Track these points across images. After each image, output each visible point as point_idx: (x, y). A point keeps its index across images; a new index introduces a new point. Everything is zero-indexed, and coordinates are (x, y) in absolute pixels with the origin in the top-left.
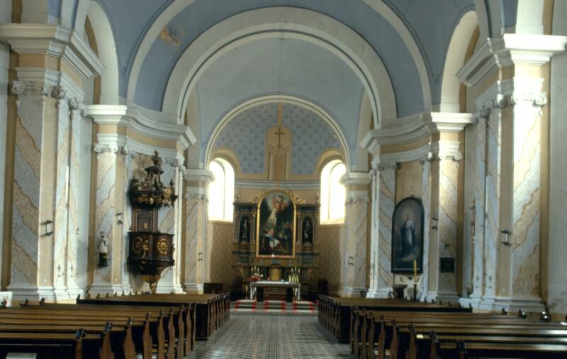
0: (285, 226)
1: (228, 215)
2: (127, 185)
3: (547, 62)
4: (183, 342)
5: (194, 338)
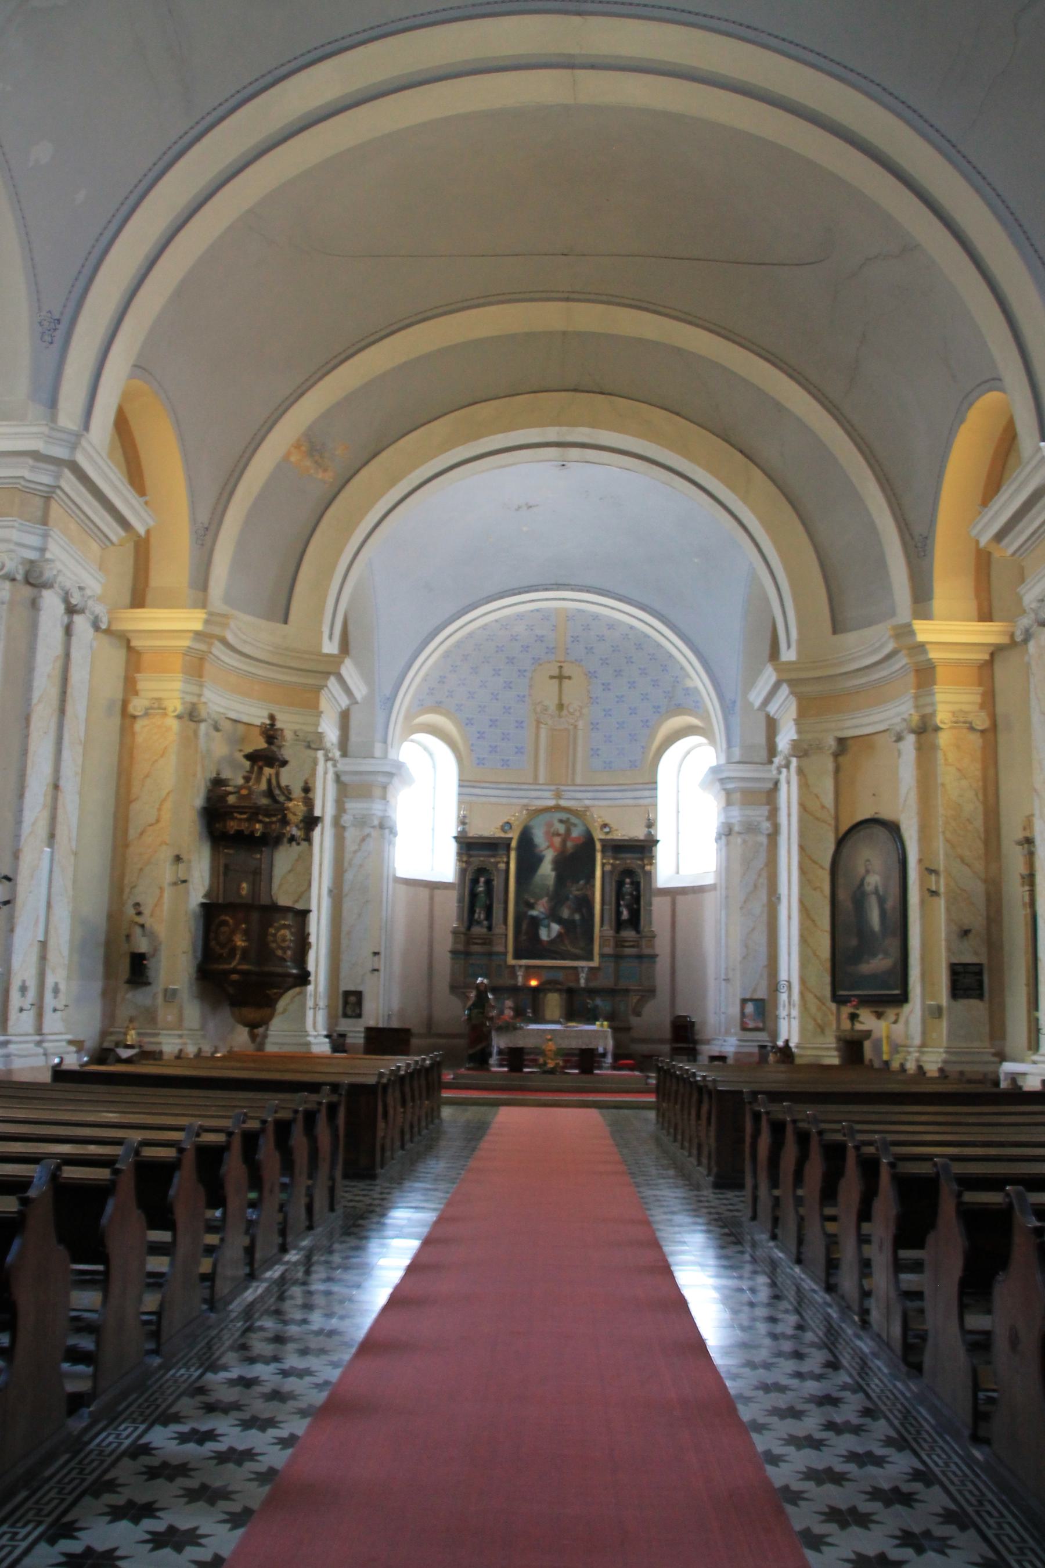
0: (575, 891)
1: (441, 864)
3: (986, 661)
4: (303, 1191)
5: (338, 1173)
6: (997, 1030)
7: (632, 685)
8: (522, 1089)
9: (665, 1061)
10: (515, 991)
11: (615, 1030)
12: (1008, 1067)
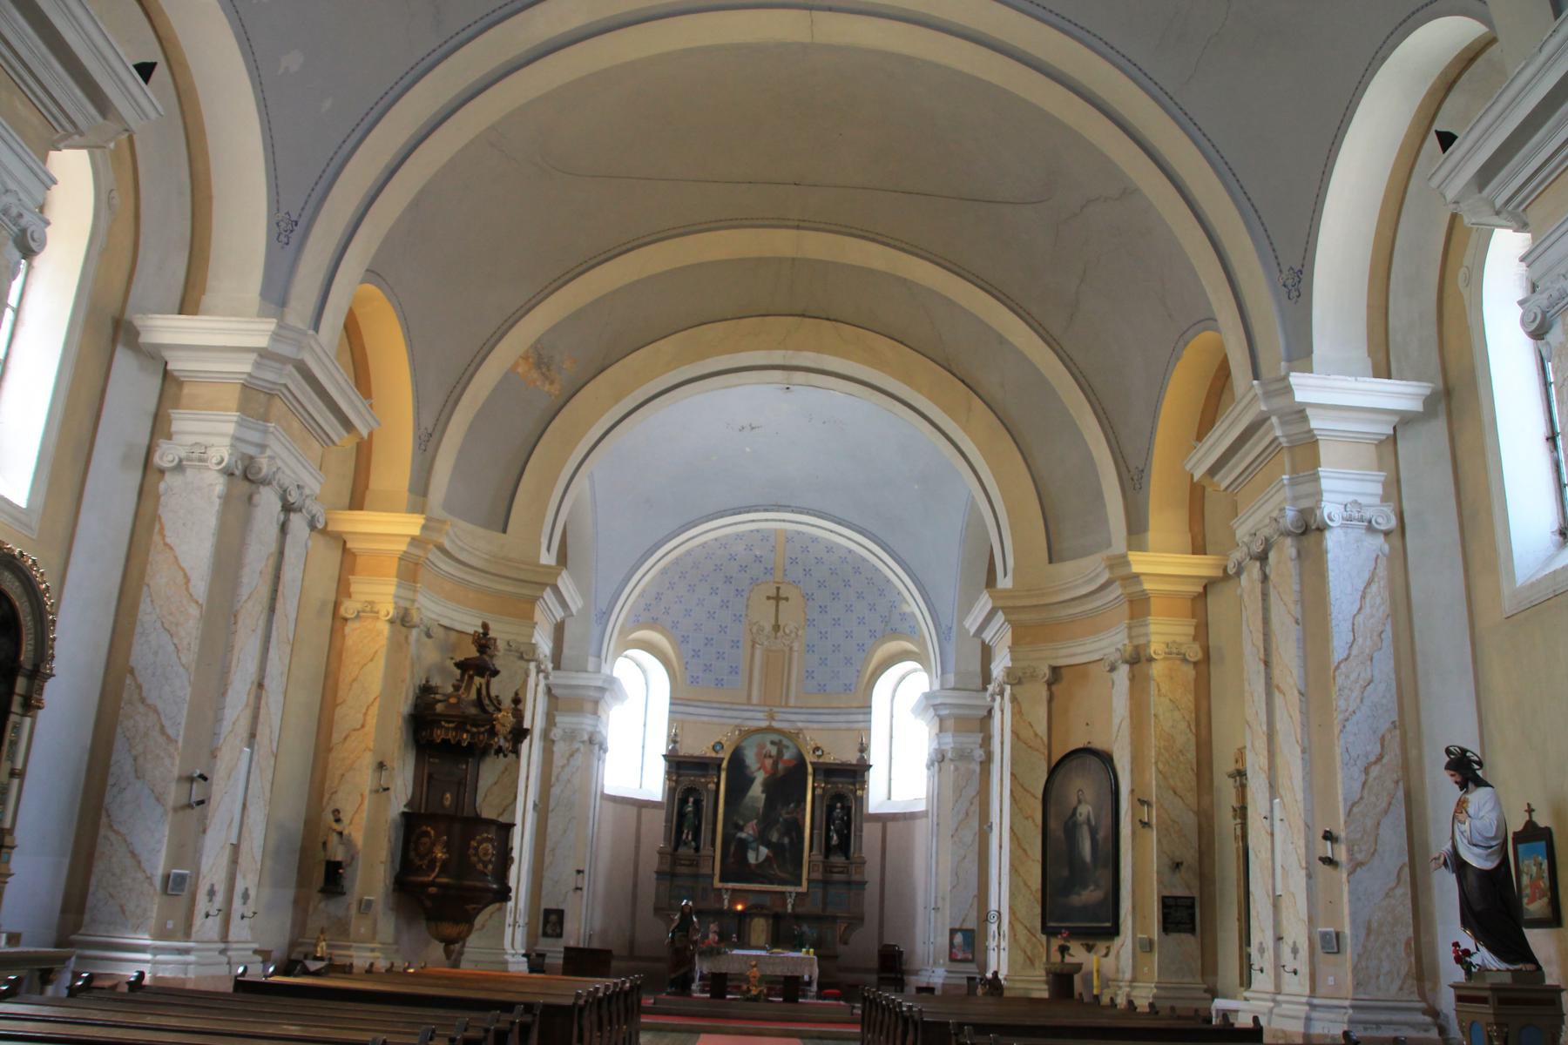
0: (784, 814)
1: (651, 784)
2: (410, 701)
3: (1388, 437)
6: (1209, 965)
7: (849, 609)
8: (727, 1017)
9: (870, 991)
10: (719, 914)
11: (821, 958)
12: (1220, 1004)
